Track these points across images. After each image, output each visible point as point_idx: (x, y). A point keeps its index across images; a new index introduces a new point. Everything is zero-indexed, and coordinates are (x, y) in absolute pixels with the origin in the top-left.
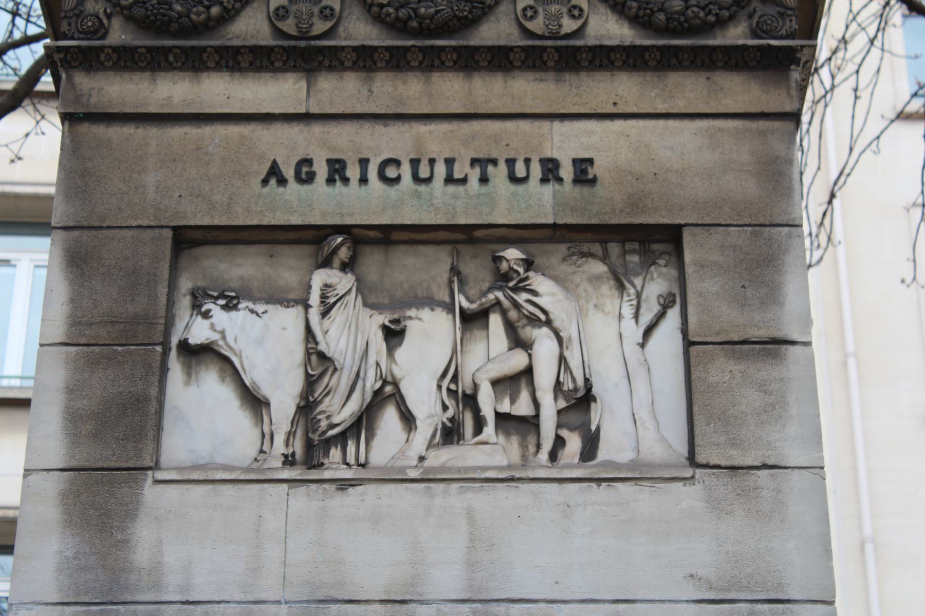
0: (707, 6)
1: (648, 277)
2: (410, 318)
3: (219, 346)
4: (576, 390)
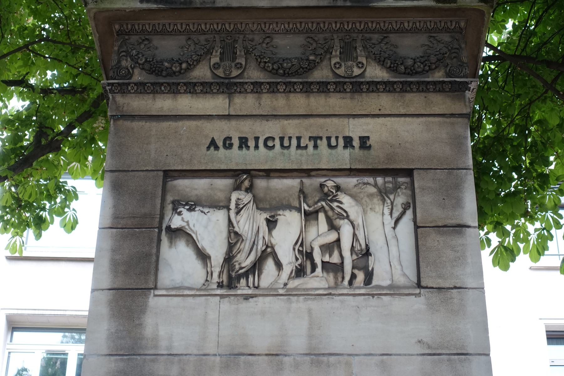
1: (397, 194)
2: (280, 215)
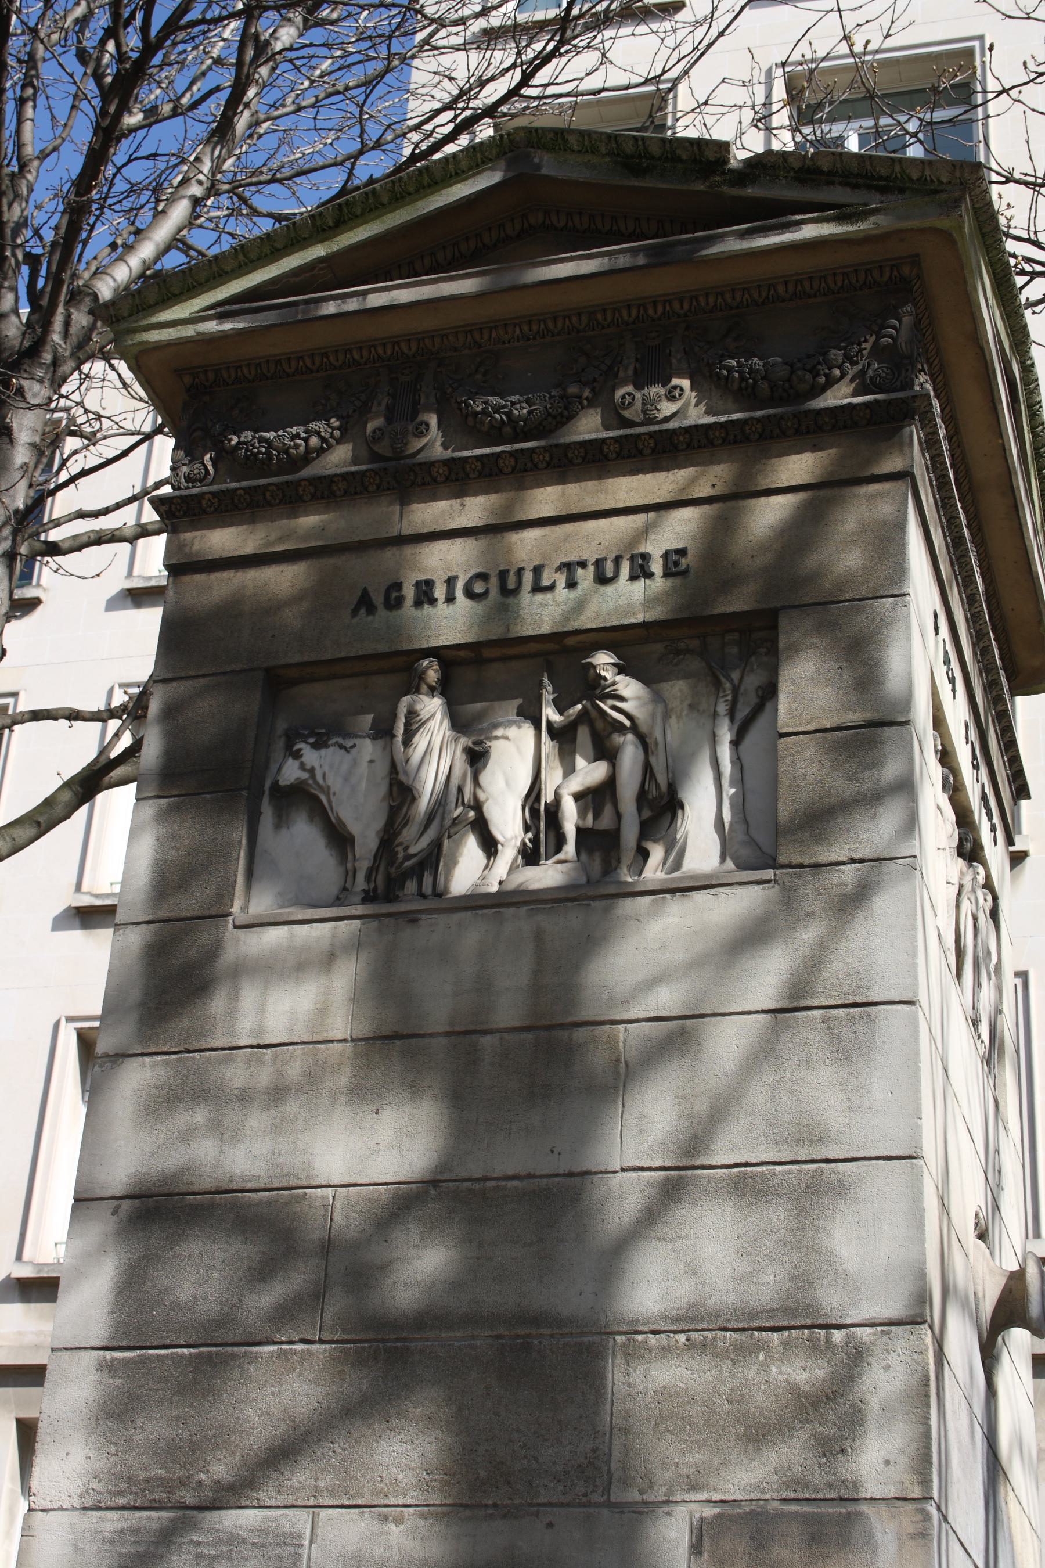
0: (814, 367)
1: (748, 669)
2: (497, 738)
3: (310, 785)
4: (661, 796)
